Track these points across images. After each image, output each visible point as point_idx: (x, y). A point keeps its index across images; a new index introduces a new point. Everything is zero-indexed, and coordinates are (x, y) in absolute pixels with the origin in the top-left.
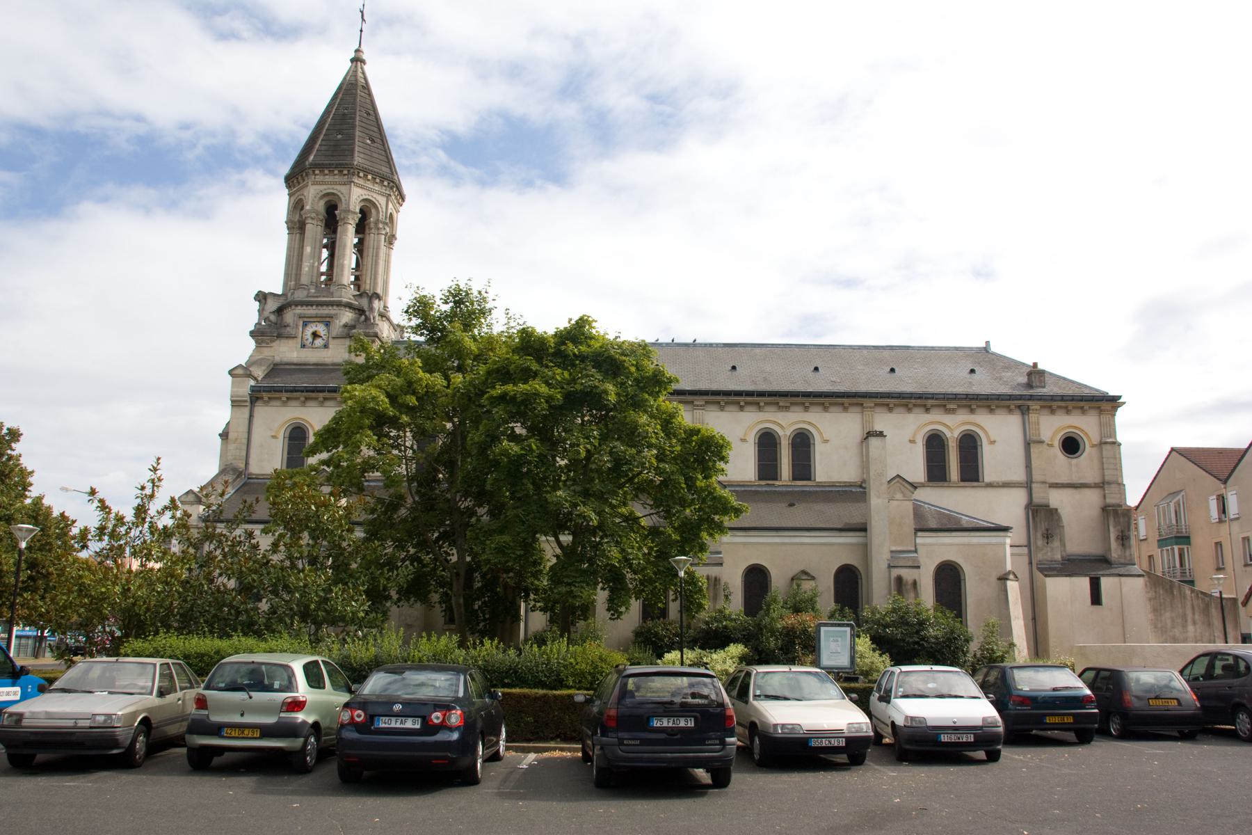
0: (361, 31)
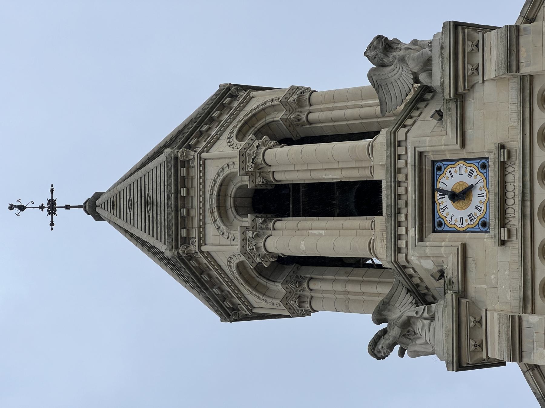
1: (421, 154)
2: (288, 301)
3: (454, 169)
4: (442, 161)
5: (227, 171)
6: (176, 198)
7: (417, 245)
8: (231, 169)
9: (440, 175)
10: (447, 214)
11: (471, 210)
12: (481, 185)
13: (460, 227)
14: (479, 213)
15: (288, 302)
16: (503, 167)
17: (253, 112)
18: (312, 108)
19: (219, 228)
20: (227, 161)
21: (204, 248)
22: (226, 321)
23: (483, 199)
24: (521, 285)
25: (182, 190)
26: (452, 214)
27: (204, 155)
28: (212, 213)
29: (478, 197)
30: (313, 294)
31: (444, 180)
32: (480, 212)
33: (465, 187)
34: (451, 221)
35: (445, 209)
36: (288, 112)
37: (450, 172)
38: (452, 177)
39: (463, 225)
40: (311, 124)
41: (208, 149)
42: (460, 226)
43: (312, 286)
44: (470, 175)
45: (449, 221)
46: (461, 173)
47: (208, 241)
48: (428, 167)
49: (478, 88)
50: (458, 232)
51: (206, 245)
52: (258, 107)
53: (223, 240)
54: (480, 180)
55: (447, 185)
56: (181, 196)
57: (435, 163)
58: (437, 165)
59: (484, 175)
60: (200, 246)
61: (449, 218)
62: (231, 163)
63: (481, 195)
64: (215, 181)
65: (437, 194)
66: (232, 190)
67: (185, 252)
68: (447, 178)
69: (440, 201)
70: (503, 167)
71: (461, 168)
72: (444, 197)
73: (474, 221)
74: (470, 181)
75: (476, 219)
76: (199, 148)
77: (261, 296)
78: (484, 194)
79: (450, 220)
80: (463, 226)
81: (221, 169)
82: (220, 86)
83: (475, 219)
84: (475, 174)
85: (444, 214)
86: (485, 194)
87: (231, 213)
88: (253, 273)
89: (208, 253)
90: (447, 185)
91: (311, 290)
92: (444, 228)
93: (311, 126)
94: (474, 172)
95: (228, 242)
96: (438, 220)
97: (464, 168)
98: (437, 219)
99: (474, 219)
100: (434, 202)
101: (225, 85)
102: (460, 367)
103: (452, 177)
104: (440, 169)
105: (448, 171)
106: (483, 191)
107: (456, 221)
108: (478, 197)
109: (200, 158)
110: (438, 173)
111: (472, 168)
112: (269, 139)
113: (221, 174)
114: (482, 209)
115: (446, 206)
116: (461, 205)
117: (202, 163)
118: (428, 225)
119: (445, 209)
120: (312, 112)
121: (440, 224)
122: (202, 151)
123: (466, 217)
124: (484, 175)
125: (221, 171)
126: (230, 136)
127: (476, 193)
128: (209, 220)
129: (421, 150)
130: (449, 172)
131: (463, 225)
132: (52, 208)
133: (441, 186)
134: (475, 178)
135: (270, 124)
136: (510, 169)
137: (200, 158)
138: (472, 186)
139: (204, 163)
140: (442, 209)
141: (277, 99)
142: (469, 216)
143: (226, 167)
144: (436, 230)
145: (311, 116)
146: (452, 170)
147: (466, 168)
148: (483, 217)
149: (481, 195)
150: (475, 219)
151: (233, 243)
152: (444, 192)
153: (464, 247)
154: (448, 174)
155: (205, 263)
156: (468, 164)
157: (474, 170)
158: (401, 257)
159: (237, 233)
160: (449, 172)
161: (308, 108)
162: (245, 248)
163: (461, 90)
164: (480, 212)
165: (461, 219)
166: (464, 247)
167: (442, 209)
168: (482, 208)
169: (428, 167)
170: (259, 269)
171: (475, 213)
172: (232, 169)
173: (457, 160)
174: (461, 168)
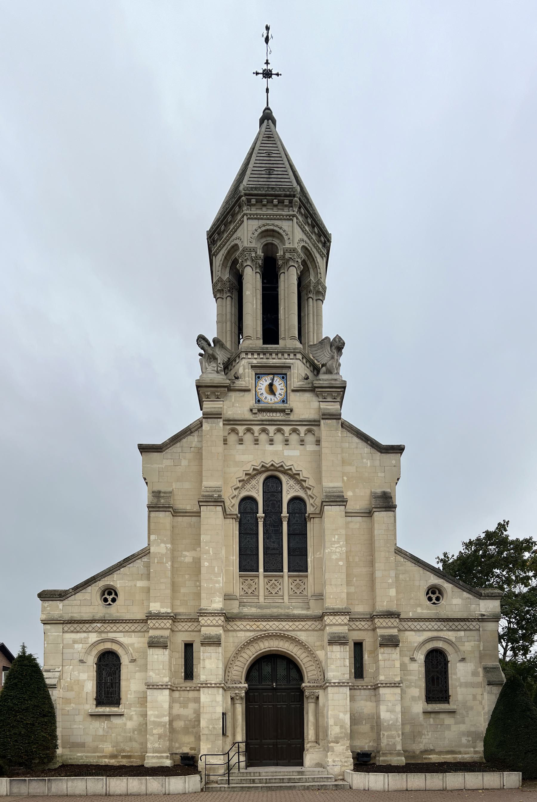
0: (267, 90)
3: (282, 386)
4: (286, 379)
5: (286, 238)
11: (265, 395)
12: (276, 400)
13: (258, 388)
14: (264, 398)
16: (282, 411)
22: (208, 235)
28: (264, 226)
30: (224, 299)
31: (278, 380)
44: (280, 394)
46: (281, 389)
48: (284, 371)
50: (256, 387)
58: (285, 376)
61: (261, 382)
63: (271, 400)
69: (269, 378)
70: (282, 411)
71: (283, 389)
74: (277, 394)
77: (221, 262)
84: (280, 397)
85: (263, 380)
89: (243, 221)
95: (249, 238)
97: (283, 391)
102: (198, 387)
104: (283, 378)
106: (273, 401)
117: (290, 218)
118: (258, 371)
121: (259, 378)
127: (272, 397)
132: (267, 74)
134: (279, 397)
136: (282, 414)
137: (294, 216)
138: (275, 395)
142: (262, 393)
145: (310, 300)
146: (282, 385)
149: (271, 400)
152: (273, 380)
153: (249, 390)
154: (281, 382)
159: (253, 245)
161: (315, 298)
163: (317, 390)
169: (284, 371)
171: (263, 397)
174: (283, 389)
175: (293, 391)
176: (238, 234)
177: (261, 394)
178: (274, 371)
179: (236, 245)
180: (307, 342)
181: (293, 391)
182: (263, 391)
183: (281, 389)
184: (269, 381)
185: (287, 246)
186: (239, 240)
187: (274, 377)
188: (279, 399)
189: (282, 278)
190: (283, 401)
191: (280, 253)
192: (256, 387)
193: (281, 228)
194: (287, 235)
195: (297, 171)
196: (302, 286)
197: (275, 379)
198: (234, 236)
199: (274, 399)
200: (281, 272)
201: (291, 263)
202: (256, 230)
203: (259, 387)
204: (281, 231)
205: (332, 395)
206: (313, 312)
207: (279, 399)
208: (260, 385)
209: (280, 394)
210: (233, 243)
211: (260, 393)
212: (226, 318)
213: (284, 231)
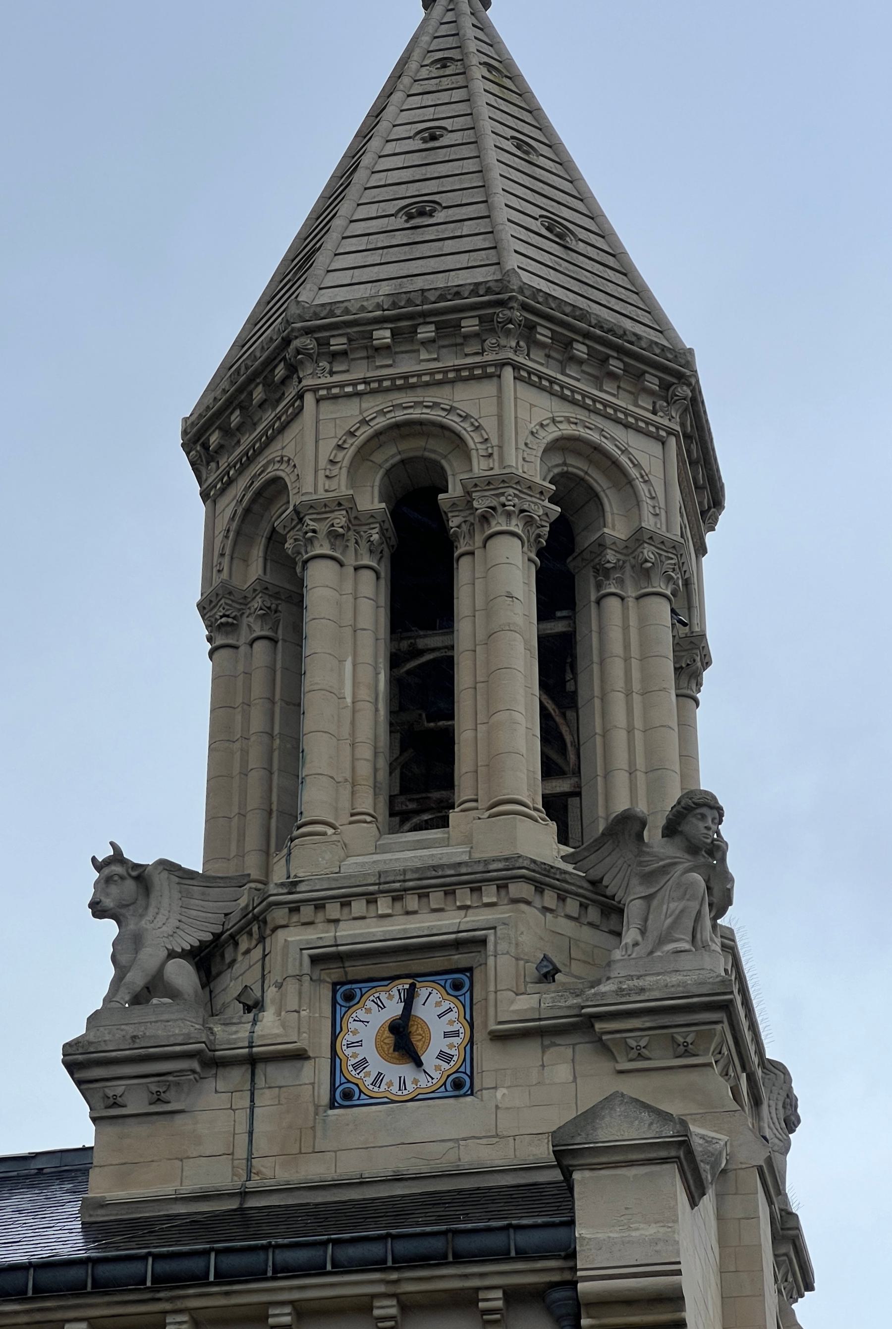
1: (483, 942)
2: (223, 597)
3: (454, 1021)
5: (472, 440)
6: (410, 316)
7: (304, 952)
8: (477, 450)
9: (444, 988)
10: (369, 1011)
11: (377, 1064)
12: (423, 1081)
14: (369, 1081)
15: (221, 599)
17: (624, 460)
18: (631, 602)
19: (352, 434)
20: (495, 441)
21: (309, 398)
22: (185, 433)
23: (395, 1089)
24: (464, 870)
25: (432, 327)
26: (368, 1022)
27: (508, 373)
29: (400, 1077)
30: (243, 649)
31: (436, 996)
32: (372, 1084)
33: (420, 1046)
34: (355, 1020)
35: (379, 1006)
36: (621, 545)
37: (450, 1009)
38: (440, 1016)
39: (347, 1047)
40: (598, 602)
41: (525, 376)
42: (344, 1042)
43: (258, 645)
44: (444, 1056)
45: (354, 1015)
46: (446, 1035)
47: (325, 406)
48: (460, 959)
49: (607, 1066)
50: (334, 1037)
51: (318, 401)
52: (637, 465)
53: (327, 449)
54: (433, 1079)
55: (424, 1004)
56: (416, 327)
57: (468, 974)
59: (441, 1086)
60: (315, 390)
61: (361, 1014)
62: (490, 451)
63: (402, 1084)
64: (451, 410)
65: (405, 984)
66: (435, 449)
67: (299, 354)
68: (438, 1004)
69: (395, 992)
71: (456, 1034)
72: (401, 1002)
73: (353, 1073)
74: (429, 1058)
75: (357, 1076)
76: (528, 355)
78: (405, 1089)
79: (357, 1019)
80: (344, 1048)
81: (477, 424)
82: (690, 349)
83: (358, 1074)
84: (445, 1066)
85: (369, 1004)
86: (405, 1092)
87: (388, 455)
88: (279, 505)
89: (301, 408)
90: (424, 1004)
91: (251, 644)
92: (341, 1006)
93: (593, 606)
94: (449, 1063)
95: (323, 463)
96: (358, 991)
97: (456, 1041)
98: (360, 989)
99: (358, 1072)
100: (393, 978)
101: (689, 364)
102: (72, 1066)
103: (440, 1016)
104: (457, 986)
105: (452, 1006)
106: (410, 1087)
107: (355, 1032)
108: (400, 1077)
109: (503, 364)
110: (449, 982)
111: (455, 1058)
112: (552, 521)
113: (466, 425)
114: (376, 1089)
115: (385, 1007)
116: (385, 1041)
119: (379, 1006)
120: (623, 605)
121: (349, 997)
122: (516, 367)
123: (362, 1052)
124: (441, 1086)
125: (472, 424)
126: (561, 422)
127: (406, 1070)
128: (371, 405)
129: (491, 940)
130: (450, 1008)
131: (347, 1047)
133: (423, 992)
134: (438, 1068)
135: (597, 500)
137: (503, 364)
138: (419, 1064)
139: (490, 376)
140: (378, 997)
141: (655, 511)
142: (365, 1060)
143: (482, 436)
144: (338, 987)
145: (613, 604)
146: (453, 1015)
147: (455, 1046)
148: (361, 1091)
149: (402, 1084)
150: (358, 1074)
151: (321, 474)
152: (409, 999)
153: (300, 1056)
154: (446, 1005)
155: (283, 394)
156: (465, 1048)
157: (452, 1063)
158: (279, 915)
159: (342, 487)
160: (450, 1008)
161: (631, 592)
162: (311, 511)
163: (598, 1026)
164: (372, 1084)
165: (360, 1043)
166: (300, 1056)
167: (378, 997)
168: (379, 1087)
169: (460, 959)
170: (275, 539)
171: (368, 1074)
172: (478, 454)
173: (471, 1025)
174: (456, 1034)
175: (500, 1038)
176: (286, 445)
177: (355, 1066)
178: (417, 966)
179: (276, 480)
180: (600, 771)
181: (500, 1038)
182: (369, 1051)
183: (446, 1035)
184: (395, 1009)
185: (480, 467)
186: (289, 470)
187: (413, 986)
188: (436, 1075)
189: (463, 572)
190: (458, 1085)
191: (455, 490)
192: (334, 1037)
193: (451, 410)
194: (477, 428)
195: (561, 143)
196: (577, 551)
197: (423, 993)
198: (275, 451)
199: (416, 1081)
200: (456, 554)
201: (499, 524)
202: (340, 447)
203: (350, 1038)
204: (452, 421)
205: (673, 1039)
206: (627, 646)
207: (436, 1075)
208: (353, 1025)
209: (444, 1056)
210: (264, 477)
211: (353, 1061)
212: (248, 689)
213: (466, 418)
